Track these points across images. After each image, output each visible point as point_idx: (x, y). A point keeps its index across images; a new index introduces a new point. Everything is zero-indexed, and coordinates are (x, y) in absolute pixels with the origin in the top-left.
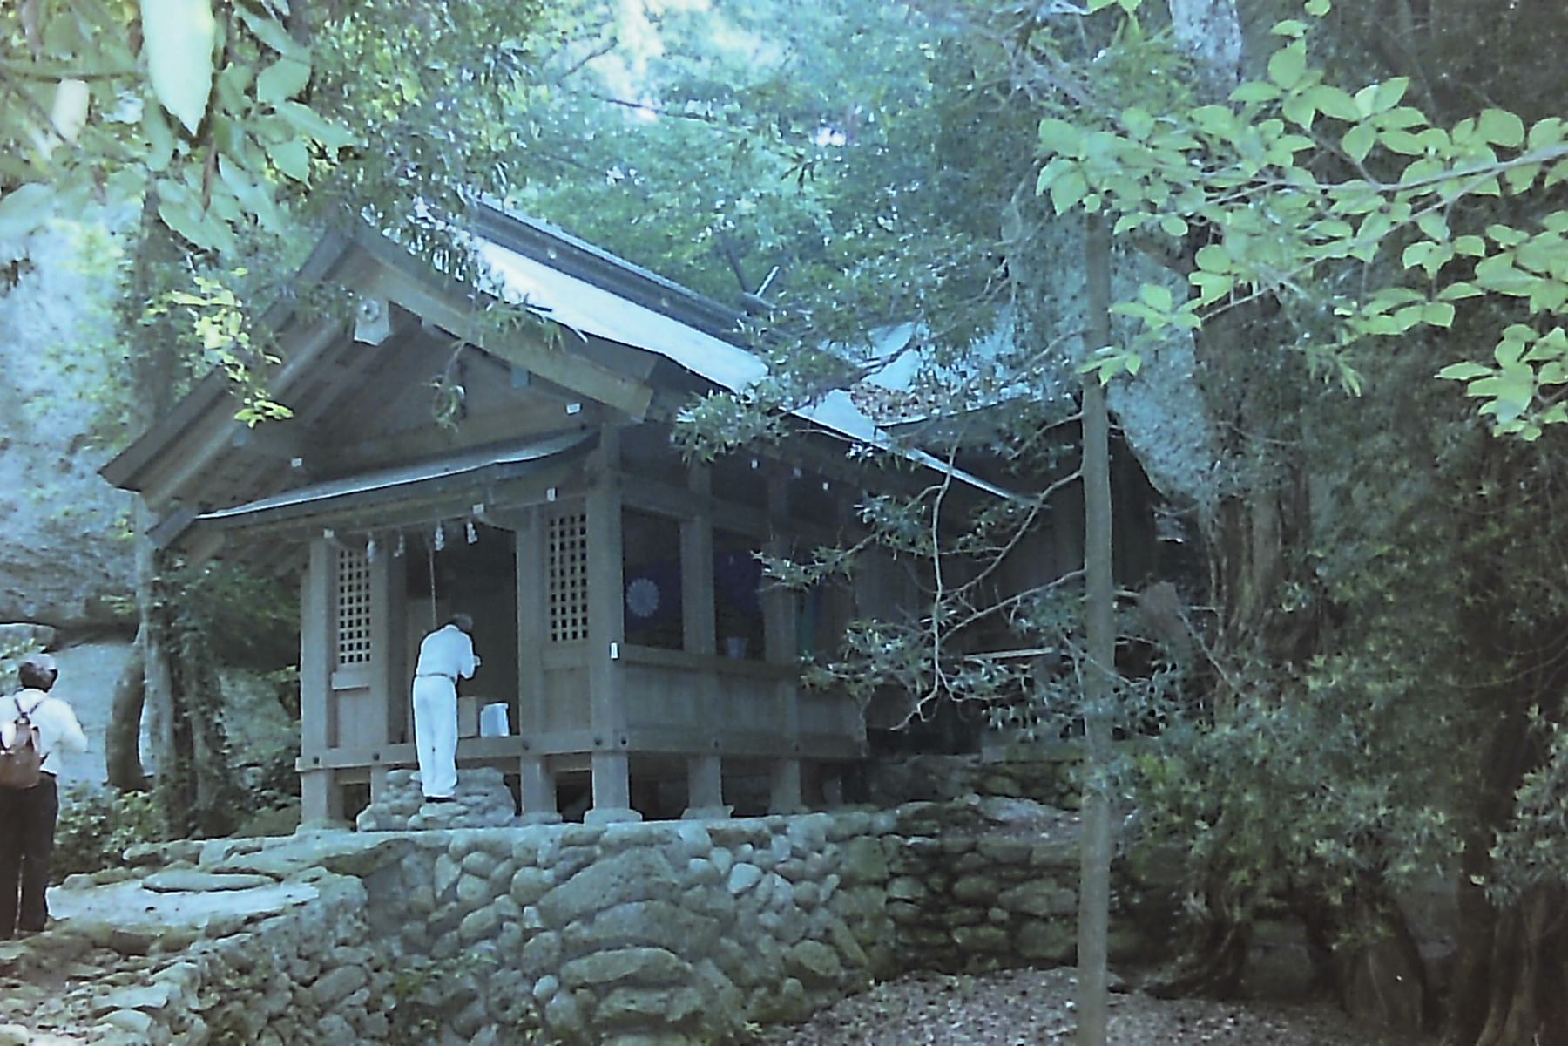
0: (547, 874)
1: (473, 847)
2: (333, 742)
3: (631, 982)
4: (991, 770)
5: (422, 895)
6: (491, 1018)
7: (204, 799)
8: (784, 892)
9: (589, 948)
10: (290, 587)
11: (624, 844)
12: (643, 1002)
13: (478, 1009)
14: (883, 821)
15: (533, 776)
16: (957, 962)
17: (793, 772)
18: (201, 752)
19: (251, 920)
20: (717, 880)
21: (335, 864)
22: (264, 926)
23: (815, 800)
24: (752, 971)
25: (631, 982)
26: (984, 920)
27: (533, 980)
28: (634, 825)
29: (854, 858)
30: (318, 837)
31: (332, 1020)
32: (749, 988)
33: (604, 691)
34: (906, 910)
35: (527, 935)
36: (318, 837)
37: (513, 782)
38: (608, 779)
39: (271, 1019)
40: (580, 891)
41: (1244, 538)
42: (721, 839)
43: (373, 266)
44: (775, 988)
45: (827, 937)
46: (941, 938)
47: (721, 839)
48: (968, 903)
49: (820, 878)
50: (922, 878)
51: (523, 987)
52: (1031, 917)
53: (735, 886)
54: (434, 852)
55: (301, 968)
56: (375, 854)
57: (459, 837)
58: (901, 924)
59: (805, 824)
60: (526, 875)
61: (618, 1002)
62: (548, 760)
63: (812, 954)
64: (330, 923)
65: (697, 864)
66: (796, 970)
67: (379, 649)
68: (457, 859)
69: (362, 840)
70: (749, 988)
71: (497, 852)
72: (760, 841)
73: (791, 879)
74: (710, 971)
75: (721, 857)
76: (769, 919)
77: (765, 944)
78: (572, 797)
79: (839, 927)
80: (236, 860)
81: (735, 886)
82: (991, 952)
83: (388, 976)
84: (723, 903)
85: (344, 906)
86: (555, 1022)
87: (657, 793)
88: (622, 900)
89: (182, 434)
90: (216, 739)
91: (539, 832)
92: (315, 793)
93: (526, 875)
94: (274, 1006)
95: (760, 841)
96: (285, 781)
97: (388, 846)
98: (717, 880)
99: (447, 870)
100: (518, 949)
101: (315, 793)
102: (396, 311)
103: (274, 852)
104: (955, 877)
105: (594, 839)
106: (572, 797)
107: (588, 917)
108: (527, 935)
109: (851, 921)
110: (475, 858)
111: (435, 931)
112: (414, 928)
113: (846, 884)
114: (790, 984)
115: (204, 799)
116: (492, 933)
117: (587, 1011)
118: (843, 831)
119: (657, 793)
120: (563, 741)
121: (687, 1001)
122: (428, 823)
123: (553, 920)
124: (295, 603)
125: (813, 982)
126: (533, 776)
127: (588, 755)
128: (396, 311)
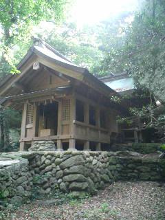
0: (61, 160)
1: (48, 154)
2: (26, 136)
3: (77, 181)
4: (130, 147)
5: (39, 163)
6: (49, 187)
7: (5, 147)
8: (101, 165)
9: (68, 174)
10: (21, 113)
11: (76, 154)
12: (78, 185)
13: (47, 185)
14: (115, 153)
15: (59, 143)
16: (129, 179)
17: (99, 145)
18: (5, 139)
19: (5, 166)
20: (91, 162)
21: (24, 157)
22: (7, 168)
23: (103, 149)
24: (96, 179)
25: (77, 181)
26: (133, 172)
27: (58, 179)
28: (75, 151)
29: (111, 160)
30: (22, 152)
31: (20, 187)
32: (95, 183)
33: (72, 128)
34: (119, 169)
35: (58, 171)
36: (22, 152)
37: (56, 144)
38: (72, 143)
39: (7, 187)
40: (67, 163)
41: (130, 144)
42: (91, 155)
43: (36, 57)
44: (99, 182)
45: (107, 174)
46: (125, 175)
47: (91, 155)
48: (130, 169)
49: (106, 163)
50: (121, 164)
51: (56, 181)
52: (142, 172)
53: (93, 163)
54: (42, 155)
55: (14, 176)
56: (31, 155)
57: (46, 153)
58: (119, 172)
59: (104, 153)
60: (58, 160)
61: (73, 185)
62: (61, 140)
63: (104, 176)
64: (21, 168)
65: (87, 159)
66: (102, 179)
67: (34, 122)
68: (46, 156)
69: (30, 152)
70: (95, 183)
71: (52, 155)
72: (97, 156)
73: (102, 162)
74: (89, 179)
75: (91, 158)
76: (99, 170)
77: (98, 174)
78: (65, 146)
79: (109, 172)
80: (7, 156)
81: (93, 163)
82: (134, 177)
83: (31, 178)
84: (92, 166)
85: (24, 164)
86: (61, 188)
87: (80, 146)
88: (75, 165)
89: (4, 84)
90: (8, 137)
91: (60, 152)
92: (22, 145)
93: (58, 160)
94: (7, 184)
95: (97, 156)
96: (18, 145)
97: (34, 154)
98: (91, 162)
99: (43, 158)
100: (55, 173)
101: (22, 145)
102: (40, 64)
103: (13, 154)
104: (128, 164)
105: (70, 153)
106: (65, 146)
107: (69, 168)
108: (58, 171)
109: (111, 171)
110: (49, 156)
111: (41, 169)
112: (37, 169)
113: (111, 164)
114: (102, 182)
115: (5, 147)
116: (51, 170)
117: (68, 186)
118: (109, 155)
119: (80, 146)
120: (64, 137)
121: (85, 185)
122: (41, 150)
123: (62, 169)
124: (21, 116)
125: (106, 182)
126: (59, 143)
127: (68, 139)
128: (40, 64)
